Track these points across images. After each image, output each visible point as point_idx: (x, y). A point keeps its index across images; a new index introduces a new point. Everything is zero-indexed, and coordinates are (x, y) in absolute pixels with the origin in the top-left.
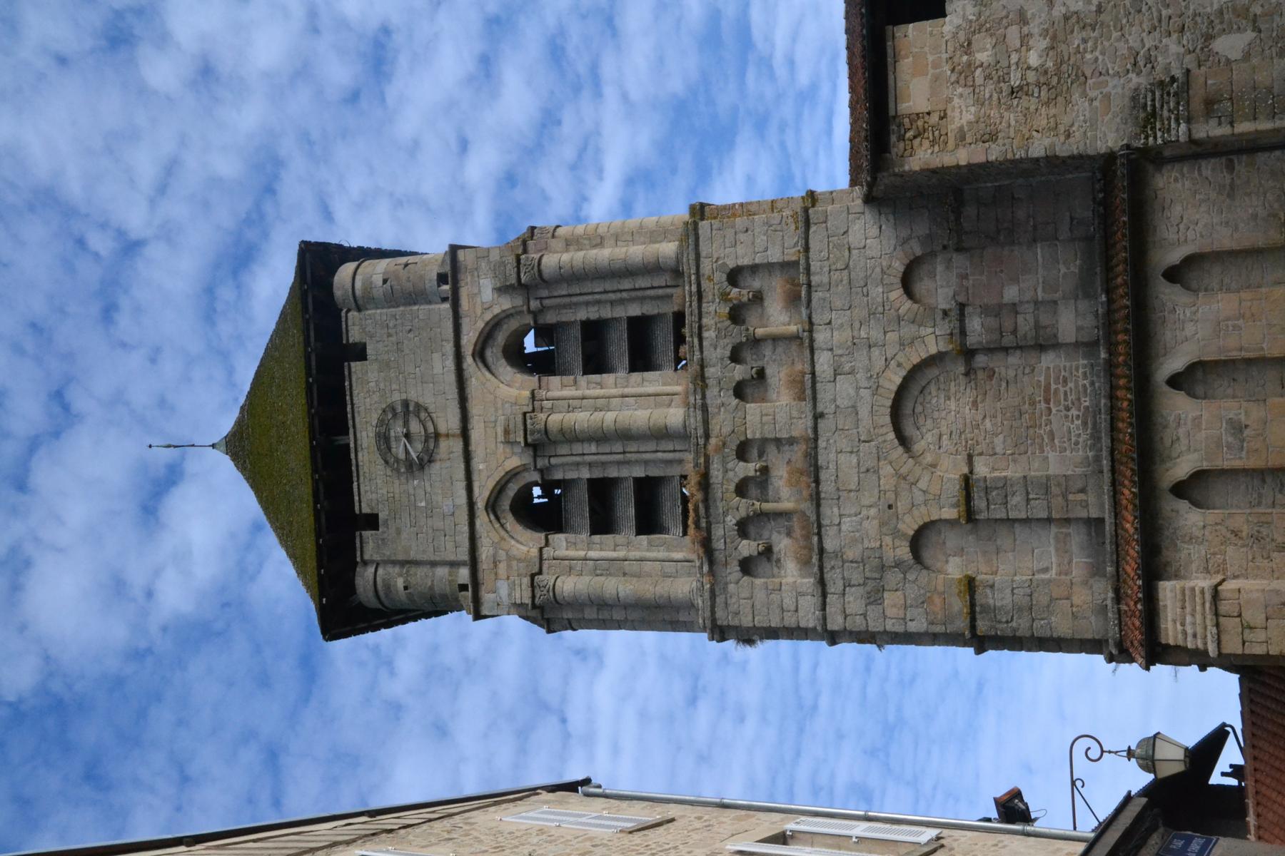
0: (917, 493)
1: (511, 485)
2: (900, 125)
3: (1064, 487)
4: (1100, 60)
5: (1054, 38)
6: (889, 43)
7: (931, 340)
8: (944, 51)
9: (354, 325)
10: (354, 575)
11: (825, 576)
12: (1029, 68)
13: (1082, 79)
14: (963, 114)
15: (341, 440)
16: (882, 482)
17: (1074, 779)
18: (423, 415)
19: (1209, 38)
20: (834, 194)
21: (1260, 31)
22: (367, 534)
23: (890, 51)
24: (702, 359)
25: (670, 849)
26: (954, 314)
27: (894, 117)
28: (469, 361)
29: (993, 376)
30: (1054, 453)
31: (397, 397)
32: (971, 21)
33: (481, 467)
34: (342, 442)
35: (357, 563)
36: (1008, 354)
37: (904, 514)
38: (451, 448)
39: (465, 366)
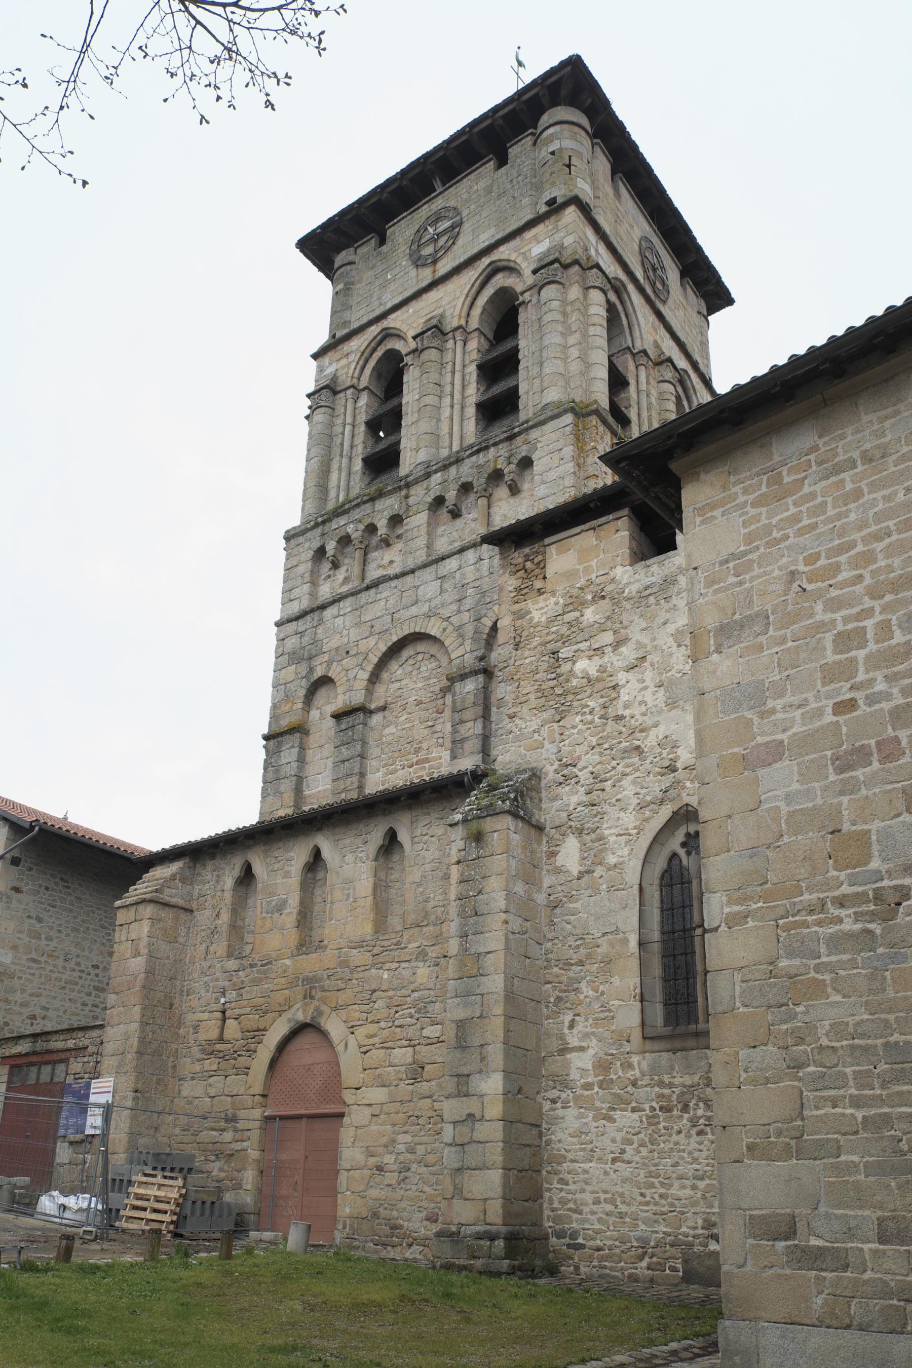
4: (573, 731)
5: (598, 680)
12: (574, 662)
13: (558, 718)
16: (365, 641)
19: (580, 832)
21: (579, 879)
23: (603, 520)
24: (463, 459)
38: (426, 276)
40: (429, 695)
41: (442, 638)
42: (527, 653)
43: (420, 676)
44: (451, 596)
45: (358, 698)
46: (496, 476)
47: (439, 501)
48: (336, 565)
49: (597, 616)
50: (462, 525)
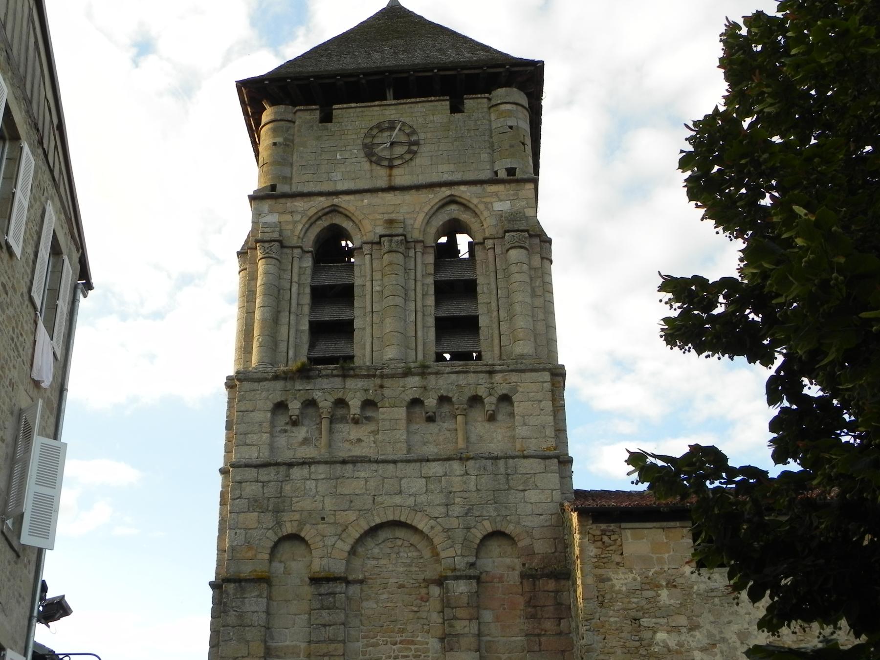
0: (333, 539)
1: (351, 224)
2: (614, 532)
3: (334, 653)
6: (678, 524)
7: (450, 552)
8: (670, 567)
9: (478, 104)
10: (286, 104)
11: (272, 467)
14: (621, 580)
15: (390, 94)
17: (70, 656)
18: (408, 157)
20: (568, 479)
22: (317, 115)
23: (672, 524)
25: (18, 351)
26: (472, 572)
27: (620, 527)
28: (446, 192)
29: (423, 601)
30: (361, 646)
31: (422, 136)
32: (692, 587)
33: (366, 201)
34: (388, 95)
35: (295, 106)
36: (439, 612)
37: (317, 530)
38: (381, 177)
39: (443, 189)
40: (411, 581)
41: (430, 535)
42: (611, 613)
43: (400, 561)
44: (439, 499)
45: (338, 568)
46: (475, 400)
47: (416, 402)
48: (295, 423)
49: (672, 601)
50: (436, 430)
